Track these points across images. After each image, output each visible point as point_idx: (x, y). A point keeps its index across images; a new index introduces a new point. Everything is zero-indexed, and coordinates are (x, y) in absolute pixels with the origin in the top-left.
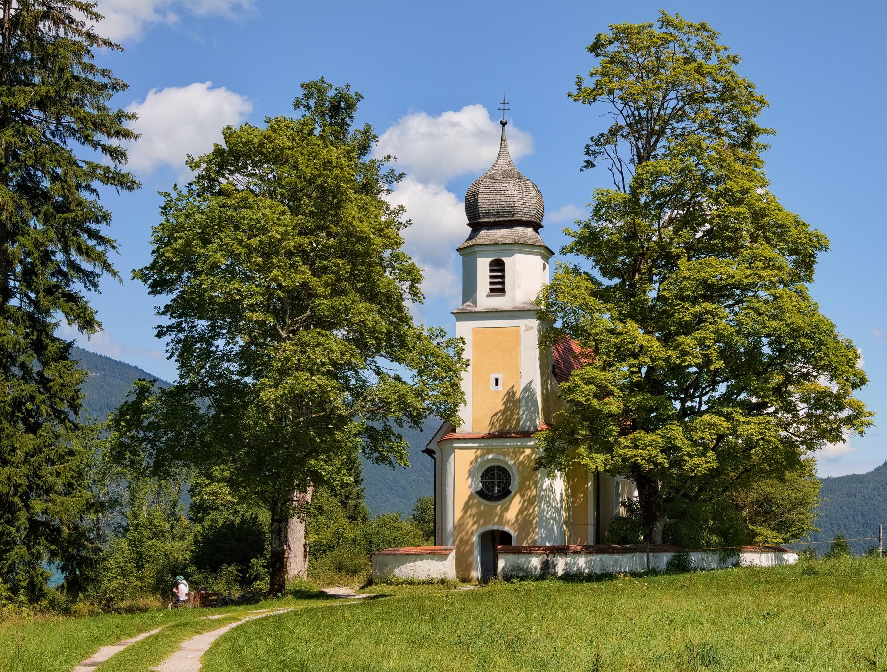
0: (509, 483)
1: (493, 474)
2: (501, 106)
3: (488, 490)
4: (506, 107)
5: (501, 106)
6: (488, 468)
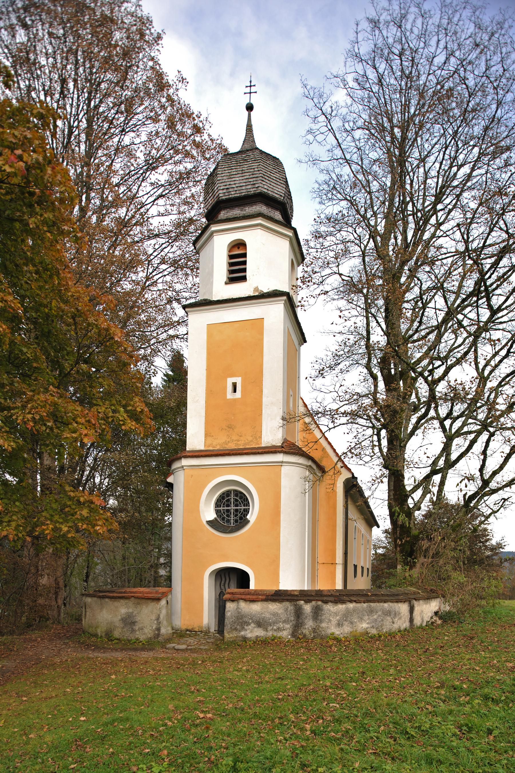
0: (247, 511)
1: (228, 500)
2: (248, 90)
3: (223, 519)
4: (253, 89)
5: (248, 90)
6: (223, 494)
